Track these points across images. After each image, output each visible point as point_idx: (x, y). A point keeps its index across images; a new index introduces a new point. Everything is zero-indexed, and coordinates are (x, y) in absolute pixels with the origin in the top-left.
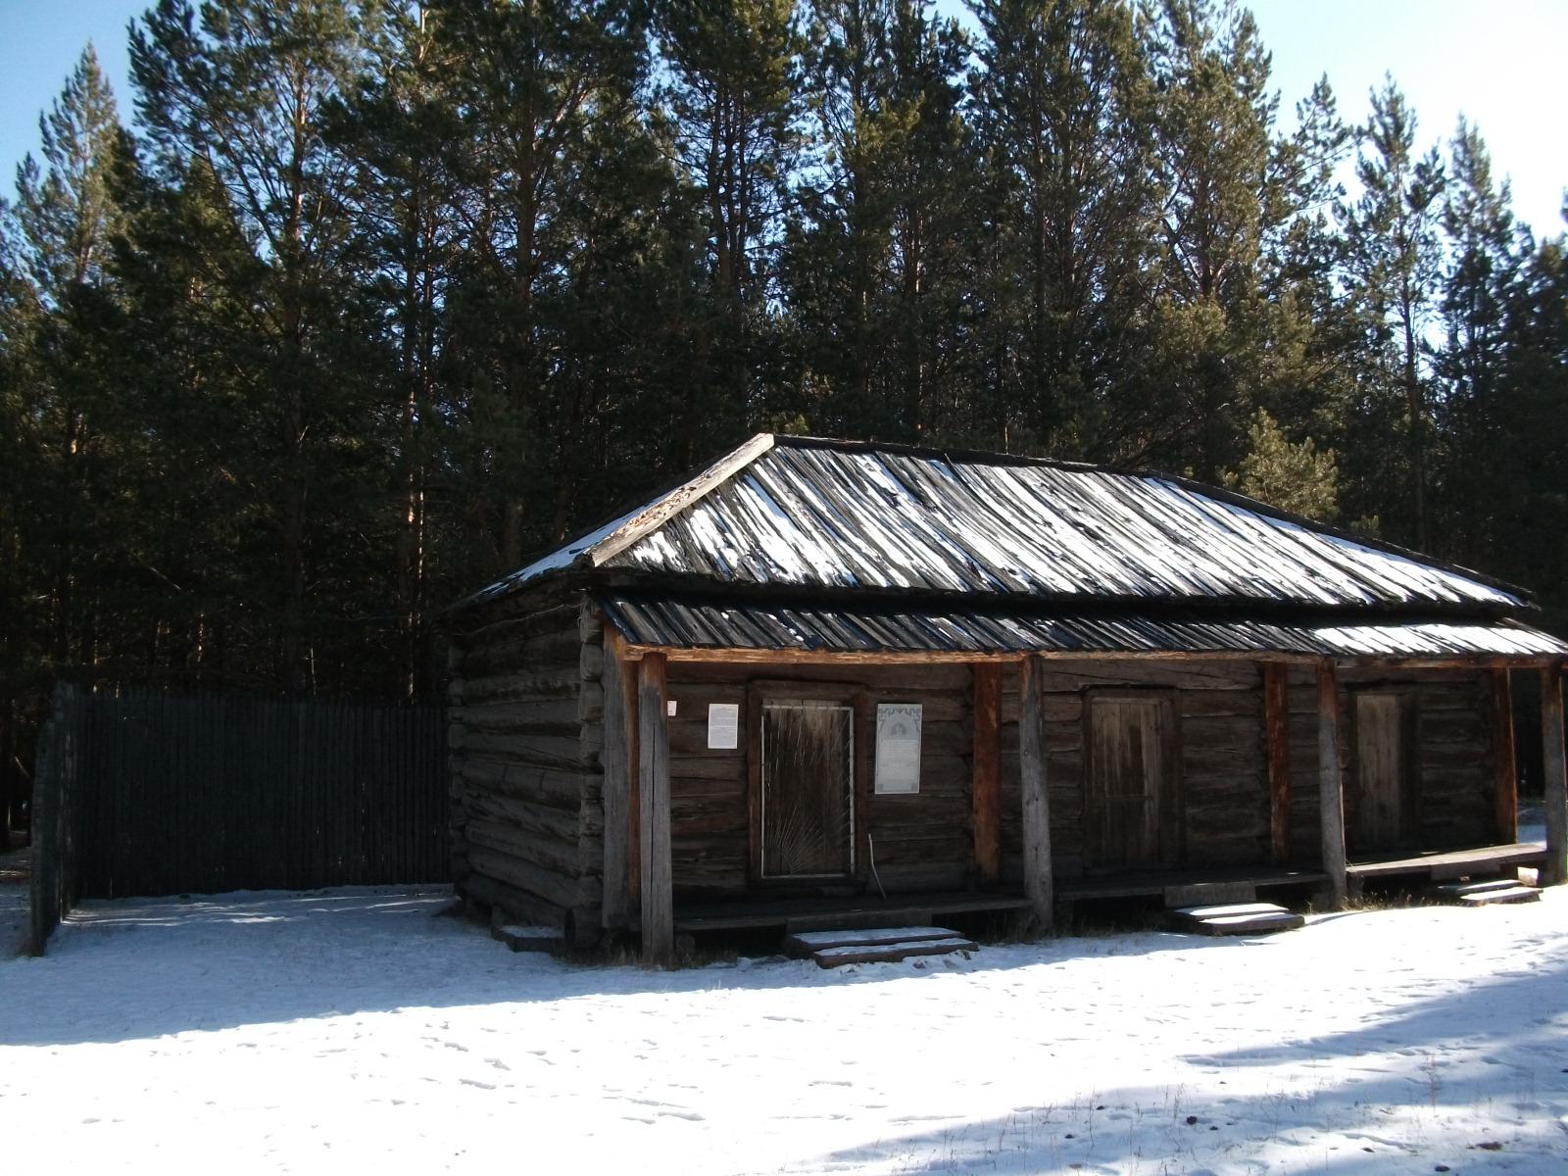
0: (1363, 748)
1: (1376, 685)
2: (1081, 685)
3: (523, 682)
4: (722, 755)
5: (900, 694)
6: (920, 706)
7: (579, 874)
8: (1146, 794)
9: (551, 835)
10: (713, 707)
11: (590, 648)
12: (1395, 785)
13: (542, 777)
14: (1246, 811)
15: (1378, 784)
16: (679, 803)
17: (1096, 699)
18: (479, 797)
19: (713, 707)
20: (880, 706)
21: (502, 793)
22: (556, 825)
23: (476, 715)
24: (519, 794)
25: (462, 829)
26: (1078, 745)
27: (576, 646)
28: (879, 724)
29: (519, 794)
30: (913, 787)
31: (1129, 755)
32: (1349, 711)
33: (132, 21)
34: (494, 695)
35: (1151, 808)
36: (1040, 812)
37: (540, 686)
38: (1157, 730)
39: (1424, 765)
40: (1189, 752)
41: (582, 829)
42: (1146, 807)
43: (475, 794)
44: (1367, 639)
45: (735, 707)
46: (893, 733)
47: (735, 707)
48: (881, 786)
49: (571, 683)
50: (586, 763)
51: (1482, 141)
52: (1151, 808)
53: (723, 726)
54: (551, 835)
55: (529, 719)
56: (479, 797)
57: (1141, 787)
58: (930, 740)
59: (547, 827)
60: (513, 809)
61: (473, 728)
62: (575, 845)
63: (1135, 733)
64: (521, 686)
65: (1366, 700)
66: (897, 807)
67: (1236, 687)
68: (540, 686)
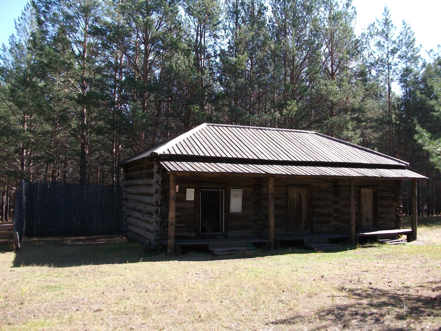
0: (363, 203)
1: (366, 186)
2: (285, 184)
3: (141, 182)
4: (190, 202)
5: (237, 187)
6: (242, 190)
7: (153, 232)
8: (303, 212)
9: (147, 222)
10: (188, 190)
11: (157, 174)
12: (371, 213)
13: (145, 207)
14: (330, 219)
15: (367, 212)
16: (178, 214)
17: (289, 188)
18: (130, 211)
19: (188, 190)
20: (231, 189)
21: (136, 211)
22: (148, 219)
23: (130, 190)
24: (140, 211)
25: (126, 219)
26: (284, 200)
27: (153, 173)
28: (231, 194)
29: (140, 211)
30: (240, 210)
31: (298, 203)
32: (359, 193)
33: (22, 11)
34: (134, 185)
35: (304, 217)
36: (41, 239)
37: (145, 183)
38: (306, 196)
39: (379, 208)
40: (315, 203)
41: (154, 221)
42: (303, 216)
43: (129, 211)
44: (186, 166)
45: (194, 190)
46: (235, 196)
47: (194, 190)
48: (232, 210)
49: (152, 183)
50: (155, 204)
51: (351, 28)
52: (304, 217)
53: (190, 195)
54: (147, 222)
55: (142, 192)
56: (130, 211)
57: (302, 212)
58: (244, 199)
59: (146, 220)
60: (138, 215)
61: (129, 193)
62: (152, 224)
63: (300, 197)
64: (140, 183)
65: (363, 191)
66: (236, 216)
67: (327, 186)
68: (145, 183)
